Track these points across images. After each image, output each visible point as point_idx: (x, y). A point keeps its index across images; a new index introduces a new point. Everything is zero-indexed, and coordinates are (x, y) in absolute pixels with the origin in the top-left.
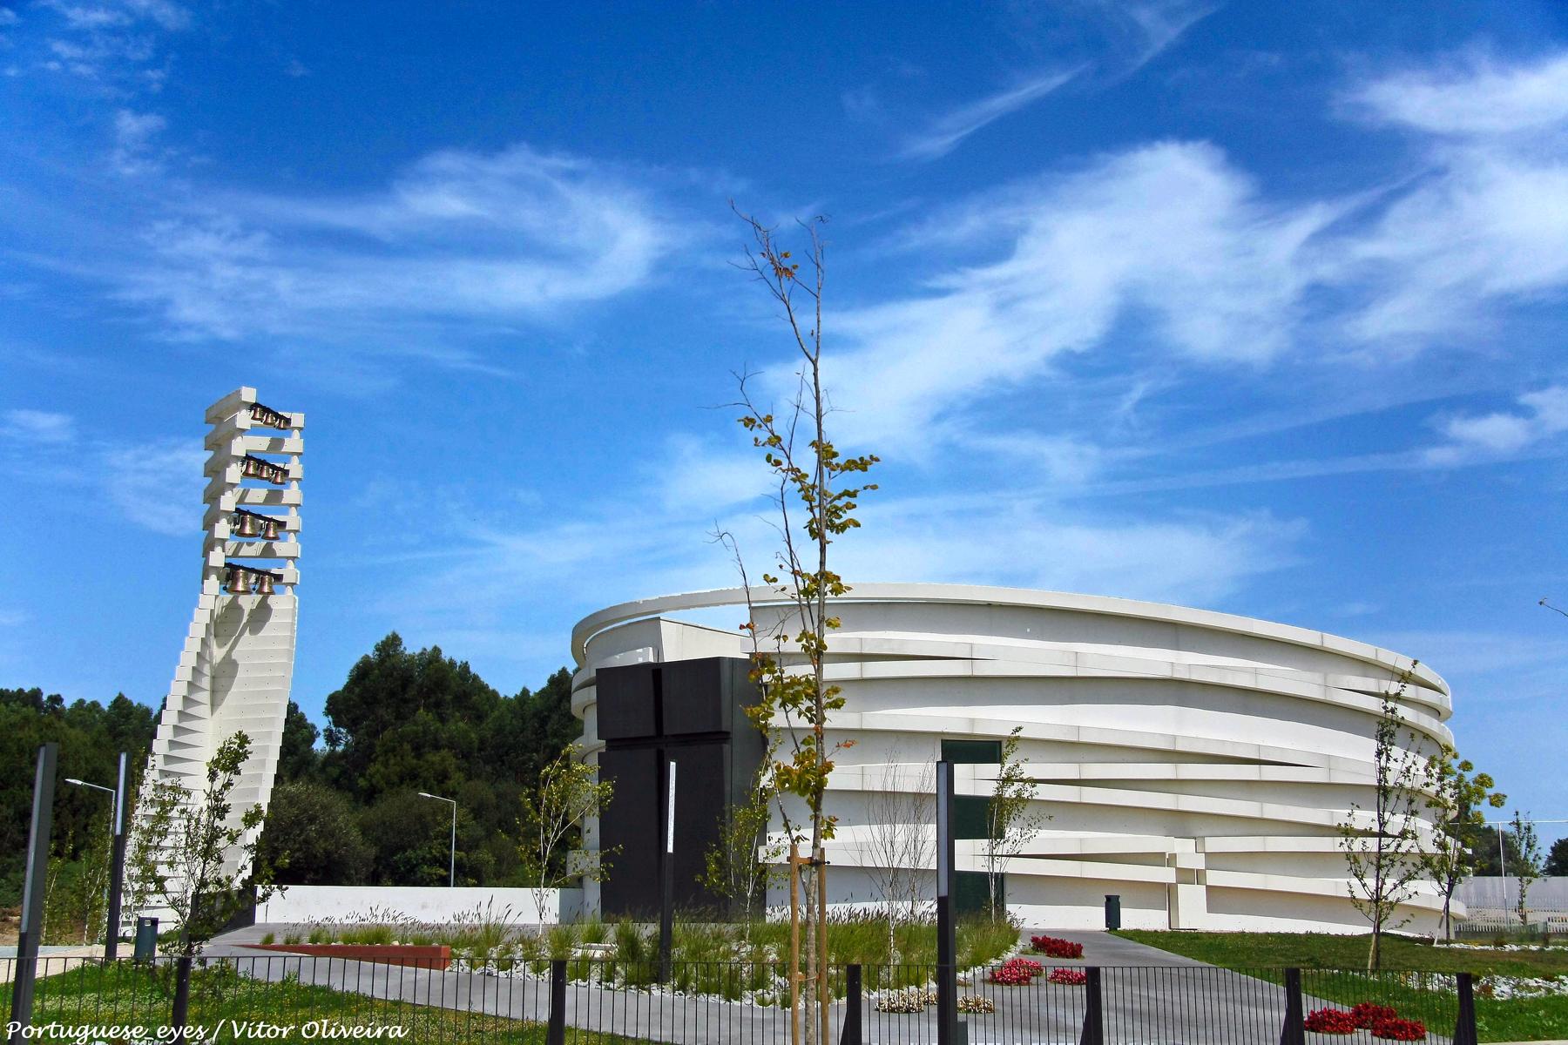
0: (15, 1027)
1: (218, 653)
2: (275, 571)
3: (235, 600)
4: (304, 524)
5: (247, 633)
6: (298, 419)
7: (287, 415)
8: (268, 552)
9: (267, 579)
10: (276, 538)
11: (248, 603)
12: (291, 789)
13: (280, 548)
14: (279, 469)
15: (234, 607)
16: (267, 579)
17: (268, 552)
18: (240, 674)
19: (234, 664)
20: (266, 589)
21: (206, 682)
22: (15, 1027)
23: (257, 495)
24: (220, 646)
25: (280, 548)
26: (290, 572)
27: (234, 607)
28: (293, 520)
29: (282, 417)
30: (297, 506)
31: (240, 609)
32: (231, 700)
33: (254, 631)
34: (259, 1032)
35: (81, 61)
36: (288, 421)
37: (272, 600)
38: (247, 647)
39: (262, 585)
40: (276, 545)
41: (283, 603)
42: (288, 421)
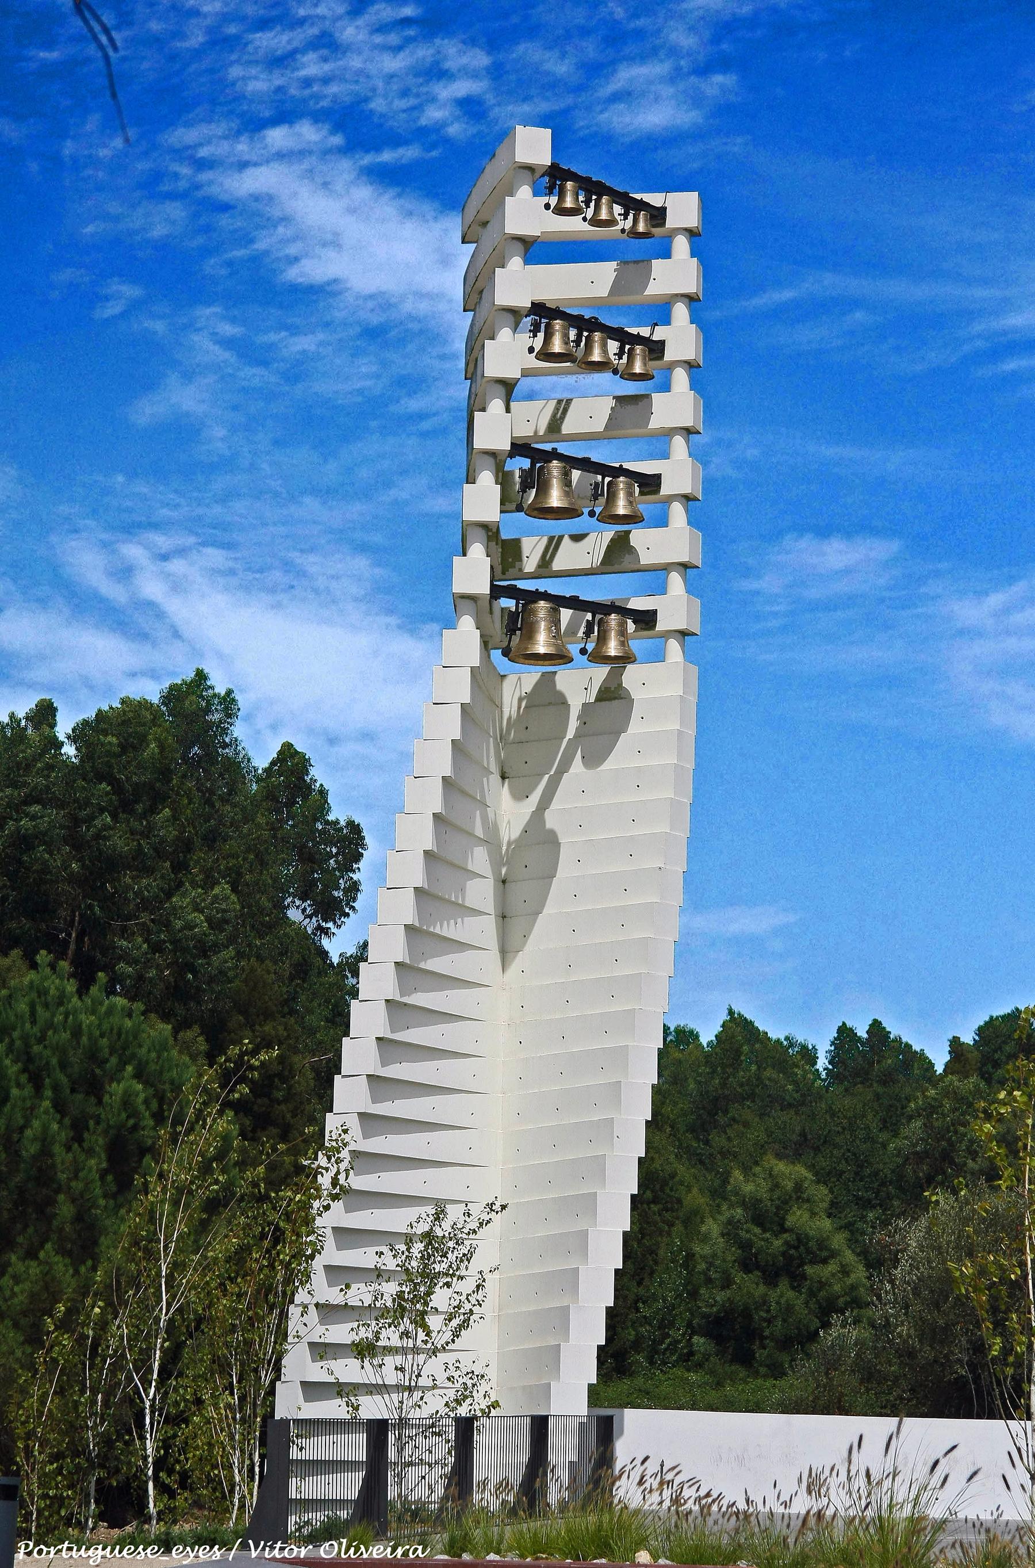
0: (27, 1546)
1: (510, 814)
2: (638, 603)
3: (548, 680)
4: (709, 483)
5: (577, 765)
6: (683, 209)
7: (655, 199)
8: (619, 551)
9: (613, 625)
10: (633, 519)
11: (579, 684)
12: (699, 922)
13: (650, 544)
14: (638, 339)
15: (546, 700)
16: (618, 491)
17: (619, 551)
18: (565, 870)
19: (552, 841)
20: (613, 648)
21: (481, 893)
22: (27, 1546)
23: (591, 411)
24: (520, 795)
25: (650, 544)
26: (675, 606)
27: (546, 700)
28: (678, 472)
29: (642, 205)
30: (685, 566)
31: (561, 702)
32: (544, 936)
33: (593, 760)
34: (276, 1551)
35: (611, 1519)
36: (658, 215)
37: (632, 677)
38: (582, 798)
39: (602, 639)
40: (638, 537)
41: (661, 686)
42: (658, 215)
